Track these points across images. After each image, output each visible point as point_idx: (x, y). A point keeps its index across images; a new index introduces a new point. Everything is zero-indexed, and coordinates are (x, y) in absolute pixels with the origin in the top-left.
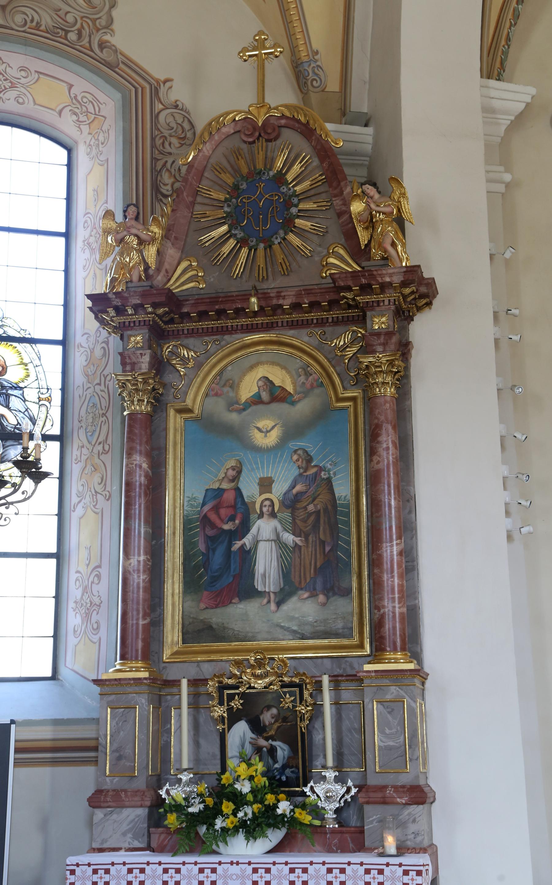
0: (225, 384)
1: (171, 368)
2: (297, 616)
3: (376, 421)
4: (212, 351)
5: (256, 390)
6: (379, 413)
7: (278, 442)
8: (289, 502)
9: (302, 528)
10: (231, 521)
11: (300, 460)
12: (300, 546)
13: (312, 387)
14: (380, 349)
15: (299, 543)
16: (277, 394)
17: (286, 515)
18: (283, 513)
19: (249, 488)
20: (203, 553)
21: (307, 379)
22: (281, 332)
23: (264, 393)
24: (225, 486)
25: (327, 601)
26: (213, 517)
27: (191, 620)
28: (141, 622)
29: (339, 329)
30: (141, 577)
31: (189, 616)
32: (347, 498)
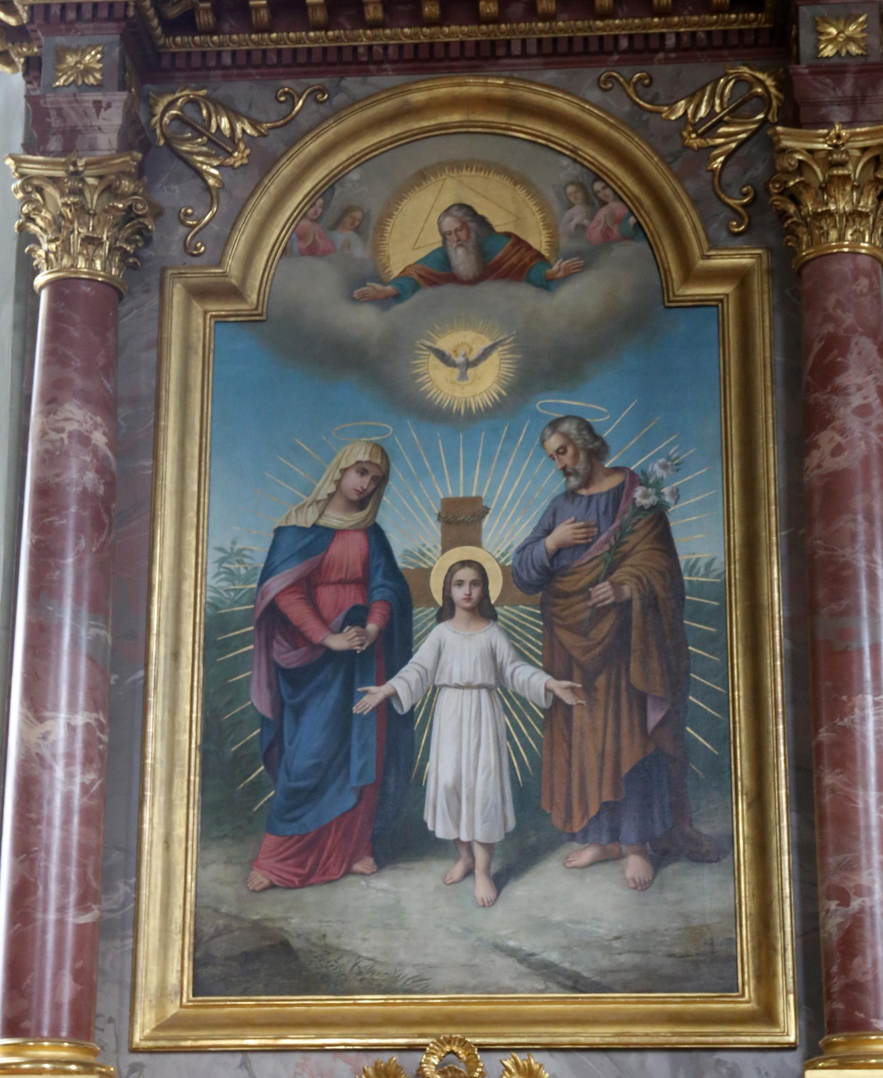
0: (337, 219)
1: (181, 166)
2: (558, 917)
3: (830, 328)
4: (304, 122)
5: (434, 241)
6: (839, 304)
7: (500, 394)
8: (533, 573)
9: (576, 654)
10: (353, 624)
11: (570, 450)
12: (569, 708)
13: (607, 239)
14: (839, 114)
15: (568, 699)
16: (500, 254)
17: (524, 612)
18: (513, 605)
19: (412, 532)
20: (263, 719)
21: (591, 216)
22: (516, 75)
23: (460, 251)
24: (335, 518)
25: (654, 878)
26: (296, 610)
27: (221, 922)
28: (72, 918)
29: (695, 71)
30: (78, 780)
31: (216, 910)
32: (713, 567)
